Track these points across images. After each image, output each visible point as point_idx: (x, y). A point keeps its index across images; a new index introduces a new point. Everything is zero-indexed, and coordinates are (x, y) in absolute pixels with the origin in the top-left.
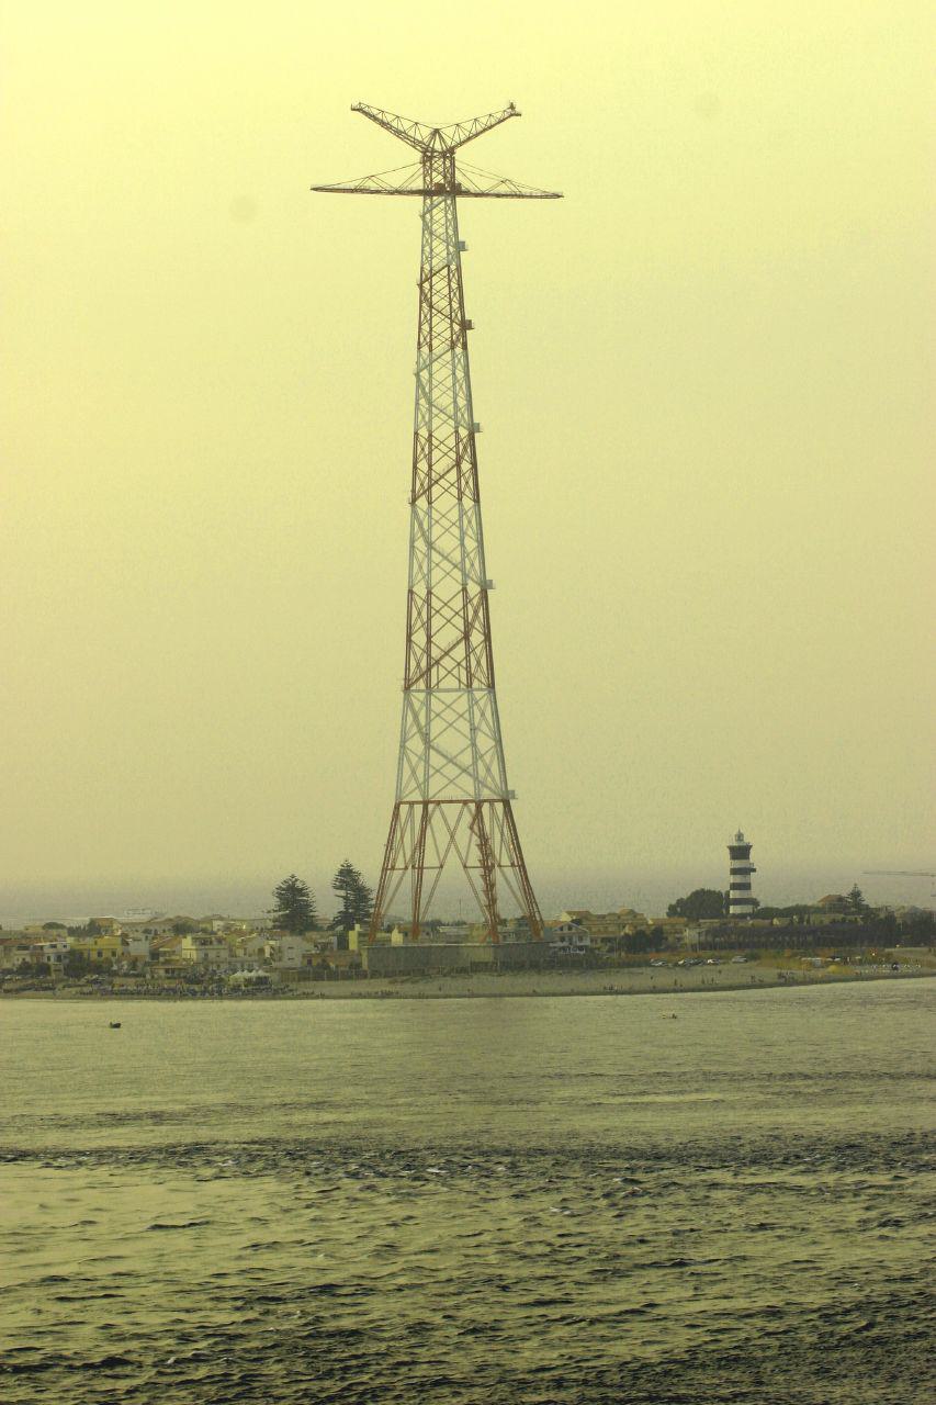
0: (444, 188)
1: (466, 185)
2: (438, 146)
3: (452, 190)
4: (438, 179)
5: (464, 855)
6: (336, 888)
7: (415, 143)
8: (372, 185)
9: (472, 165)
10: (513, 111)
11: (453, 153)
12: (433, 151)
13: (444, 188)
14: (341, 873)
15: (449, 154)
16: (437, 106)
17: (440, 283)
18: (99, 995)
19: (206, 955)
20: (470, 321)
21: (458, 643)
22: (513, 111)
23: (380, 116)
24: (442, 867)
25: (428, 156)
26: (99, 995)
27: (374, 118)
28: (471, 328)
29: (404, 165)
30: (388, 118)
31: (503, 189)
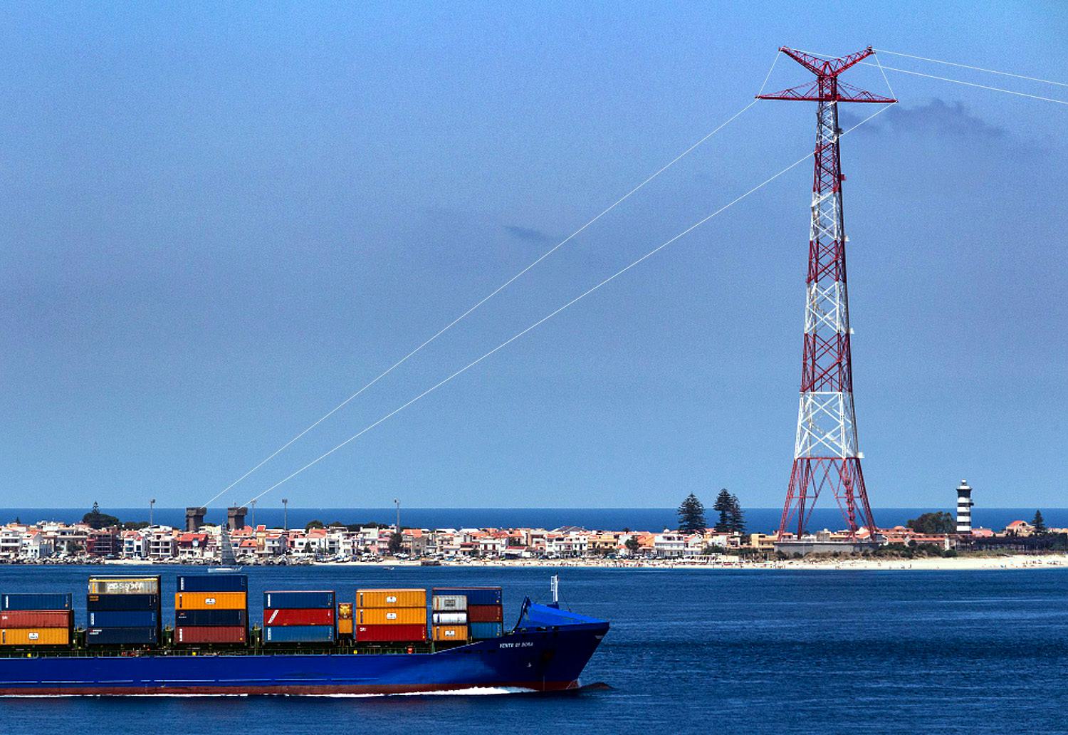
0: (828, 88)
1: (844, 95)
2: (828, 71)
3: (835, 96)
4: (827, 91)
5: (817, 489)
6: (716, 509)
7: (814, 70)
8: (789, 95)
9: (849, 82)
10: (870, 52)
11: (837, 76)
12: (825, 75)
13: (828, 88)
14: (719, 499)
15: (834, 78)
16: (826, 52)
17: (827, 154)
18: (944, 513)
19: (799, 538)
20: (843, 175)
21: (835, 365)
22: (870, 52)
23: (795, 54)
24: (817, 496)
25: (821, 77)
26: (944, 513)
27: (792, 56)
28: (843, 179)
29: (806, 82)
30: (799, 56)
31: (864, 97)
